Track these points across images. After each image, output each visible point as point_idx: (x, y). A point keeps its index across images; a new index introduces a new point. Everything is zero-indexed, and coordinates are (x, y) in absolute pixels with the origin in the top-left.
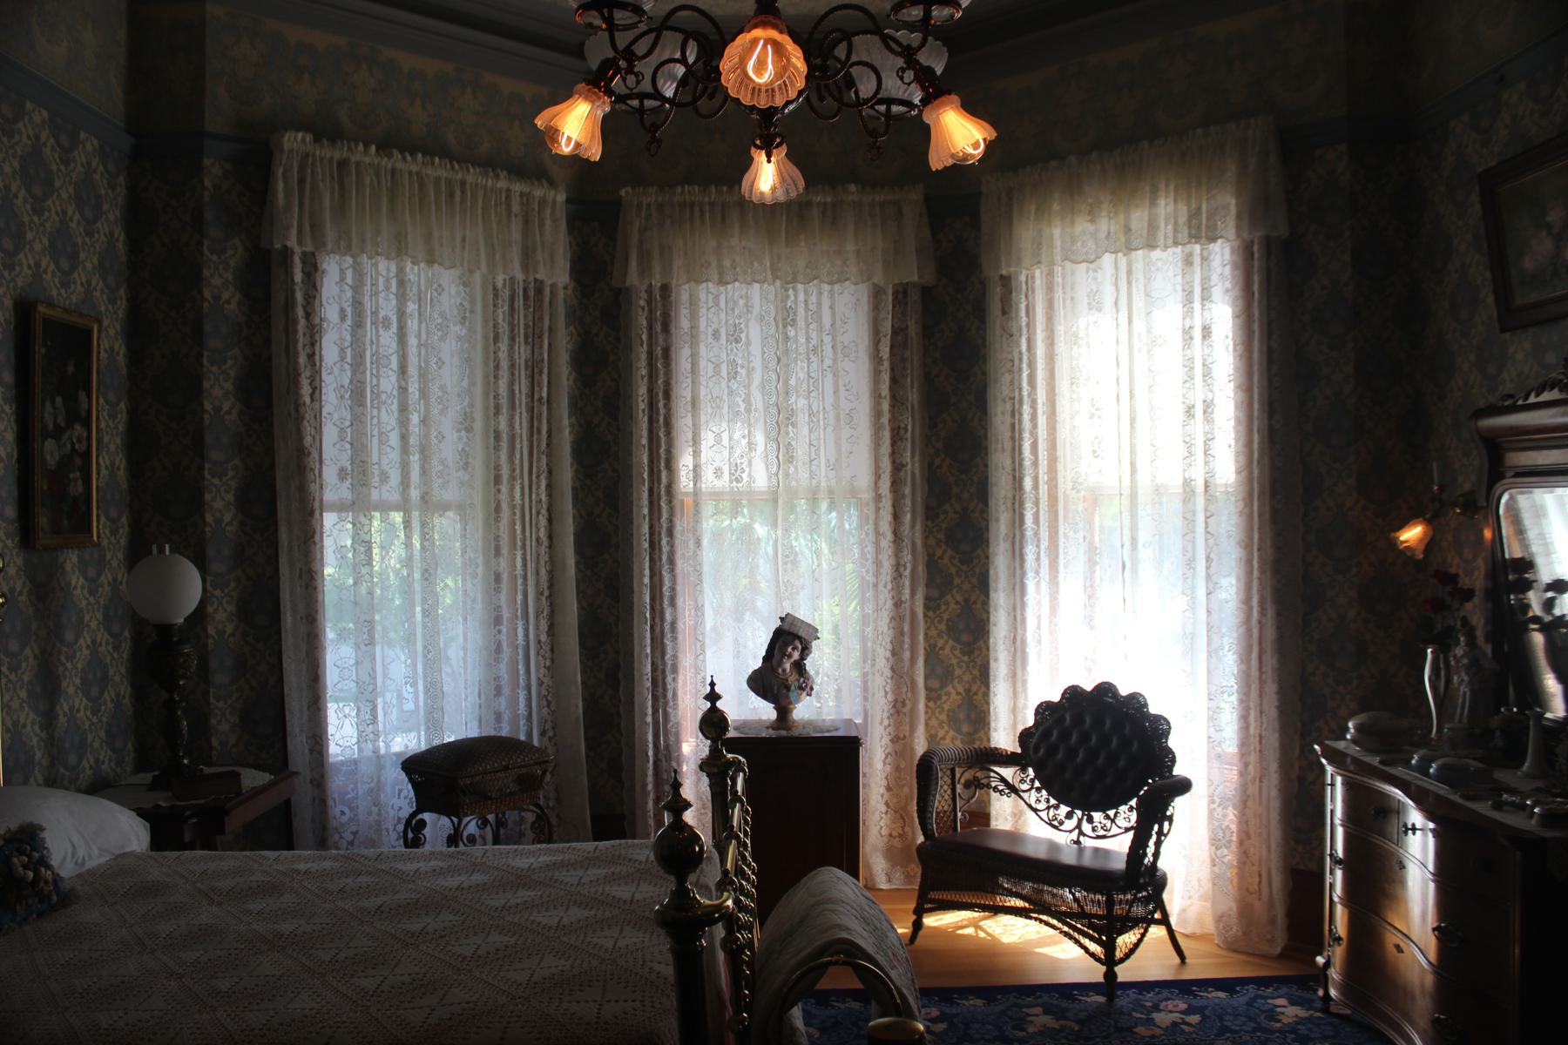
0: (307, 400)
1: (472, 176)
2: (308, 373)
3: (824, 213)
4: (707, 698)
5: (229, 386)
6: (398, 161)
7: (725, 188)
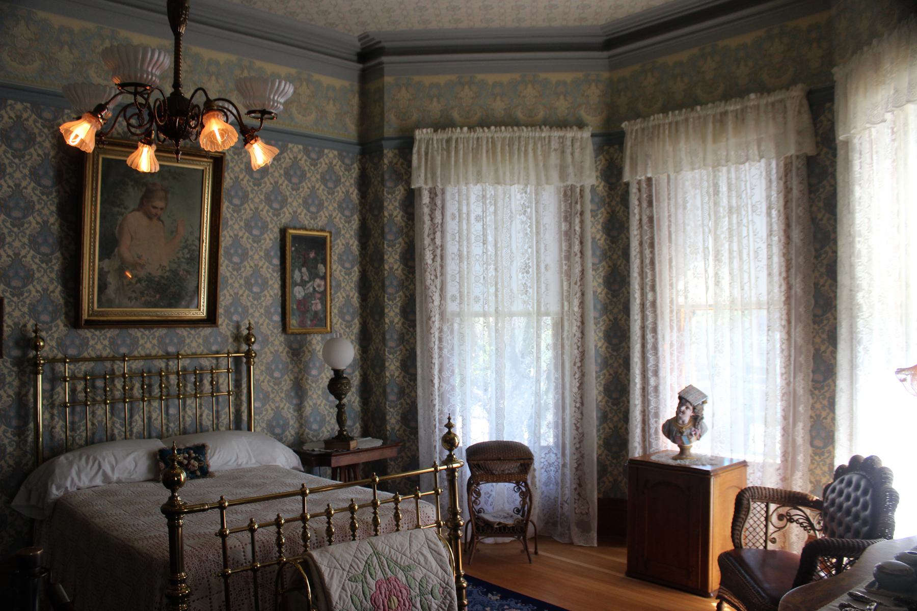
0: (429, 262)
1: (526, 132)
2: (431, 248)
3: (737, 117)
4: (446, 426)
5: (397, 257)
6: (480, 133)
7: (677, 112)
